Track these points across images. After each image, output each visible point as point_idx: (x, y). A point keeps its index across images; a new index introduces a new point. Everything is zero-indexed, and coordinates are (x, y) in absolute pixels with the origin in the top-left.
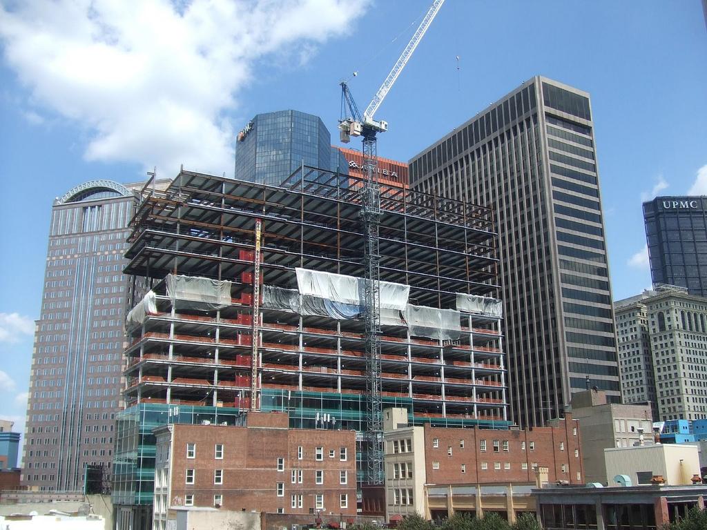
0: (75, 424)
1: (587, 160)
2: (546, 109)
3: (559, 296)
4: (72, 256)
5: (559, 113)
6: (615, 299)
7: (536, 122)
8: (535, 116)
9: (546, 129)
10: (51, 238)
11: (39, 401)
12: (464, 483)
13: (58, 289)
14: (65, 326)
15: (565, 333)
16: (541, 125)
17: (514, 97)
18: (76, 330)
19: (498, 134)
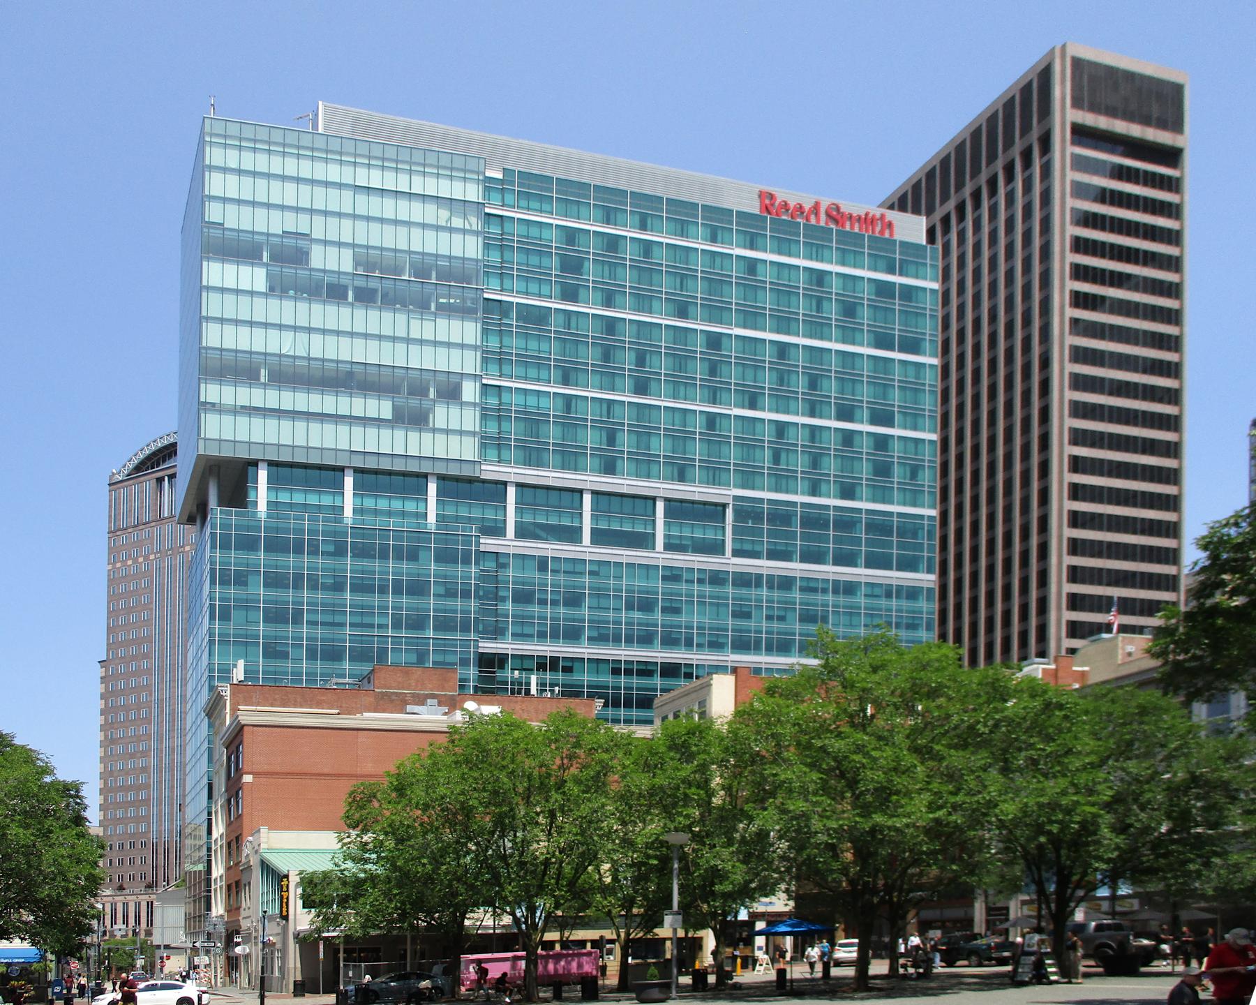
0: (118, 517)
4: (146, 558)
5: (1102, 122)
8: (1046, 142)
10: (111, 535)
11: (115, 774)
13: (129, 610)
14: (144, 664)
17: (997, 111)
18: (160, 701)
19: (951, 205)
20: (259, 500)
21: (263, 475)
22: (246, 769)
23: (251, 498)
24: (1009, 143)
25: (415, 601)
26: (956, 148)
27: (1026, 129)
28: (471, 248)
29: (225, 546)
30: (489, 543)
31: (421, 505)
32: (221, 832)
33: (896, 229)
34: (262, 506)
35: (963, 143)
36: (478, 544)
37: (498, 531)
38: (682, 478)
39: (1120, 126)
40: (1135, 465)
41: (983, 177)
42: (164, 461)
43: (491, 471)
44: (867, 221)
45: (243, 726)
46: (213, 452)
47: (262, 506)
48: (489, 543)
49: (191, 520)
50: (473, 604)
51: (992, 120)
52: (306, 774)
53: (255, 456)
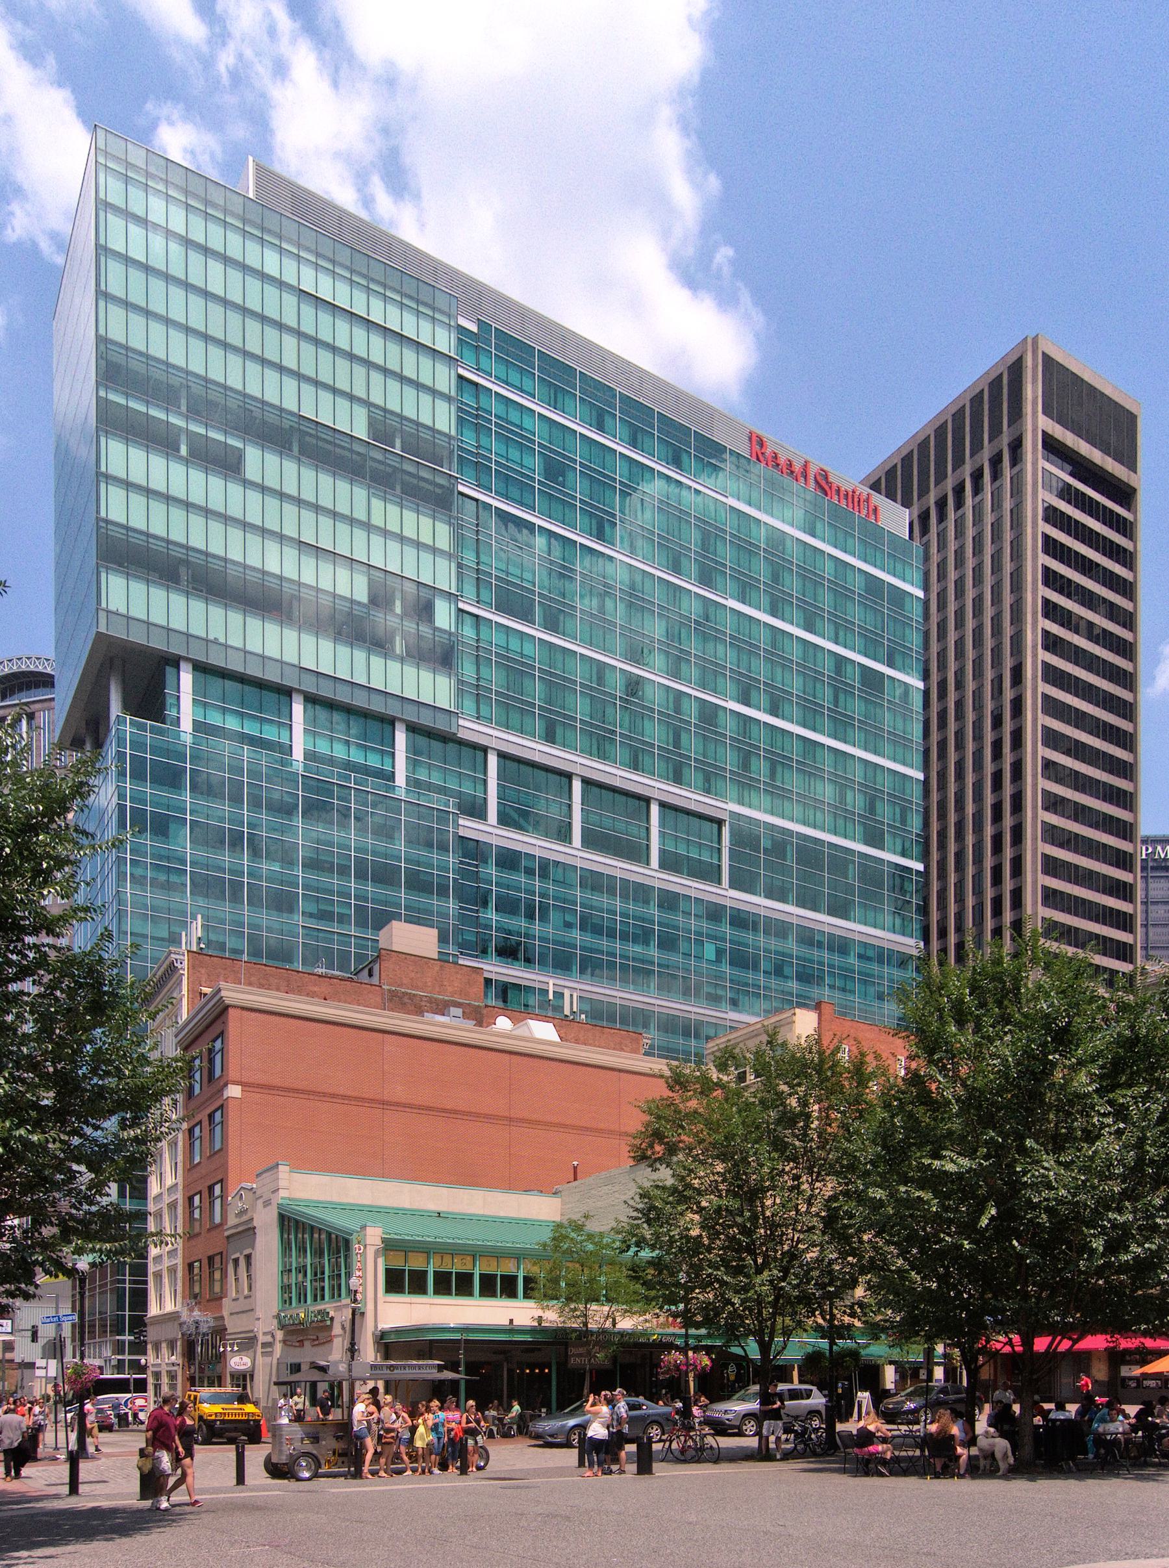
1: (1118, 569)
2: (1045, 423)
3: (1035, 413)
5: (1069, 439)
6: (1147, 826)
7: (1016, 459)
8: (1016, 446)
9: (1040, 474)
12: (602, 1126)
15: (1040, 728)
16: (1029, 530)
17: (964, 406)
20: (182, 716)
21: (187, 678)
22: (233, 1073)
23: (171, 712)
24: (977, 447)
25: (383, 891)
26: (903, 459)
27: (996, 432)
28: (444, 419)
29: (138, 775)
30: (469, 827)
31: (387, 760)
32: (169, 1181)
33: (881, 516)
34: (186, 725)
35: (927, 439)
36: (456, 823)
37: (477, 810)
38: (678, 779)
39: (1084, 448)
40: (1076, 851)
41: (950, 483)
42: (12, 693)
43: (470, 728)
44: (851, 497)
45: (227, 1007)
46: (118, 632)
47: (186, 725)
48: (469, 827)
49: (77, 743)
50: (452, 905)
51: (958, 416)
52: (314, 1093)
53: (176, 649)
